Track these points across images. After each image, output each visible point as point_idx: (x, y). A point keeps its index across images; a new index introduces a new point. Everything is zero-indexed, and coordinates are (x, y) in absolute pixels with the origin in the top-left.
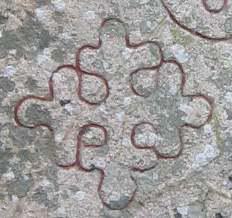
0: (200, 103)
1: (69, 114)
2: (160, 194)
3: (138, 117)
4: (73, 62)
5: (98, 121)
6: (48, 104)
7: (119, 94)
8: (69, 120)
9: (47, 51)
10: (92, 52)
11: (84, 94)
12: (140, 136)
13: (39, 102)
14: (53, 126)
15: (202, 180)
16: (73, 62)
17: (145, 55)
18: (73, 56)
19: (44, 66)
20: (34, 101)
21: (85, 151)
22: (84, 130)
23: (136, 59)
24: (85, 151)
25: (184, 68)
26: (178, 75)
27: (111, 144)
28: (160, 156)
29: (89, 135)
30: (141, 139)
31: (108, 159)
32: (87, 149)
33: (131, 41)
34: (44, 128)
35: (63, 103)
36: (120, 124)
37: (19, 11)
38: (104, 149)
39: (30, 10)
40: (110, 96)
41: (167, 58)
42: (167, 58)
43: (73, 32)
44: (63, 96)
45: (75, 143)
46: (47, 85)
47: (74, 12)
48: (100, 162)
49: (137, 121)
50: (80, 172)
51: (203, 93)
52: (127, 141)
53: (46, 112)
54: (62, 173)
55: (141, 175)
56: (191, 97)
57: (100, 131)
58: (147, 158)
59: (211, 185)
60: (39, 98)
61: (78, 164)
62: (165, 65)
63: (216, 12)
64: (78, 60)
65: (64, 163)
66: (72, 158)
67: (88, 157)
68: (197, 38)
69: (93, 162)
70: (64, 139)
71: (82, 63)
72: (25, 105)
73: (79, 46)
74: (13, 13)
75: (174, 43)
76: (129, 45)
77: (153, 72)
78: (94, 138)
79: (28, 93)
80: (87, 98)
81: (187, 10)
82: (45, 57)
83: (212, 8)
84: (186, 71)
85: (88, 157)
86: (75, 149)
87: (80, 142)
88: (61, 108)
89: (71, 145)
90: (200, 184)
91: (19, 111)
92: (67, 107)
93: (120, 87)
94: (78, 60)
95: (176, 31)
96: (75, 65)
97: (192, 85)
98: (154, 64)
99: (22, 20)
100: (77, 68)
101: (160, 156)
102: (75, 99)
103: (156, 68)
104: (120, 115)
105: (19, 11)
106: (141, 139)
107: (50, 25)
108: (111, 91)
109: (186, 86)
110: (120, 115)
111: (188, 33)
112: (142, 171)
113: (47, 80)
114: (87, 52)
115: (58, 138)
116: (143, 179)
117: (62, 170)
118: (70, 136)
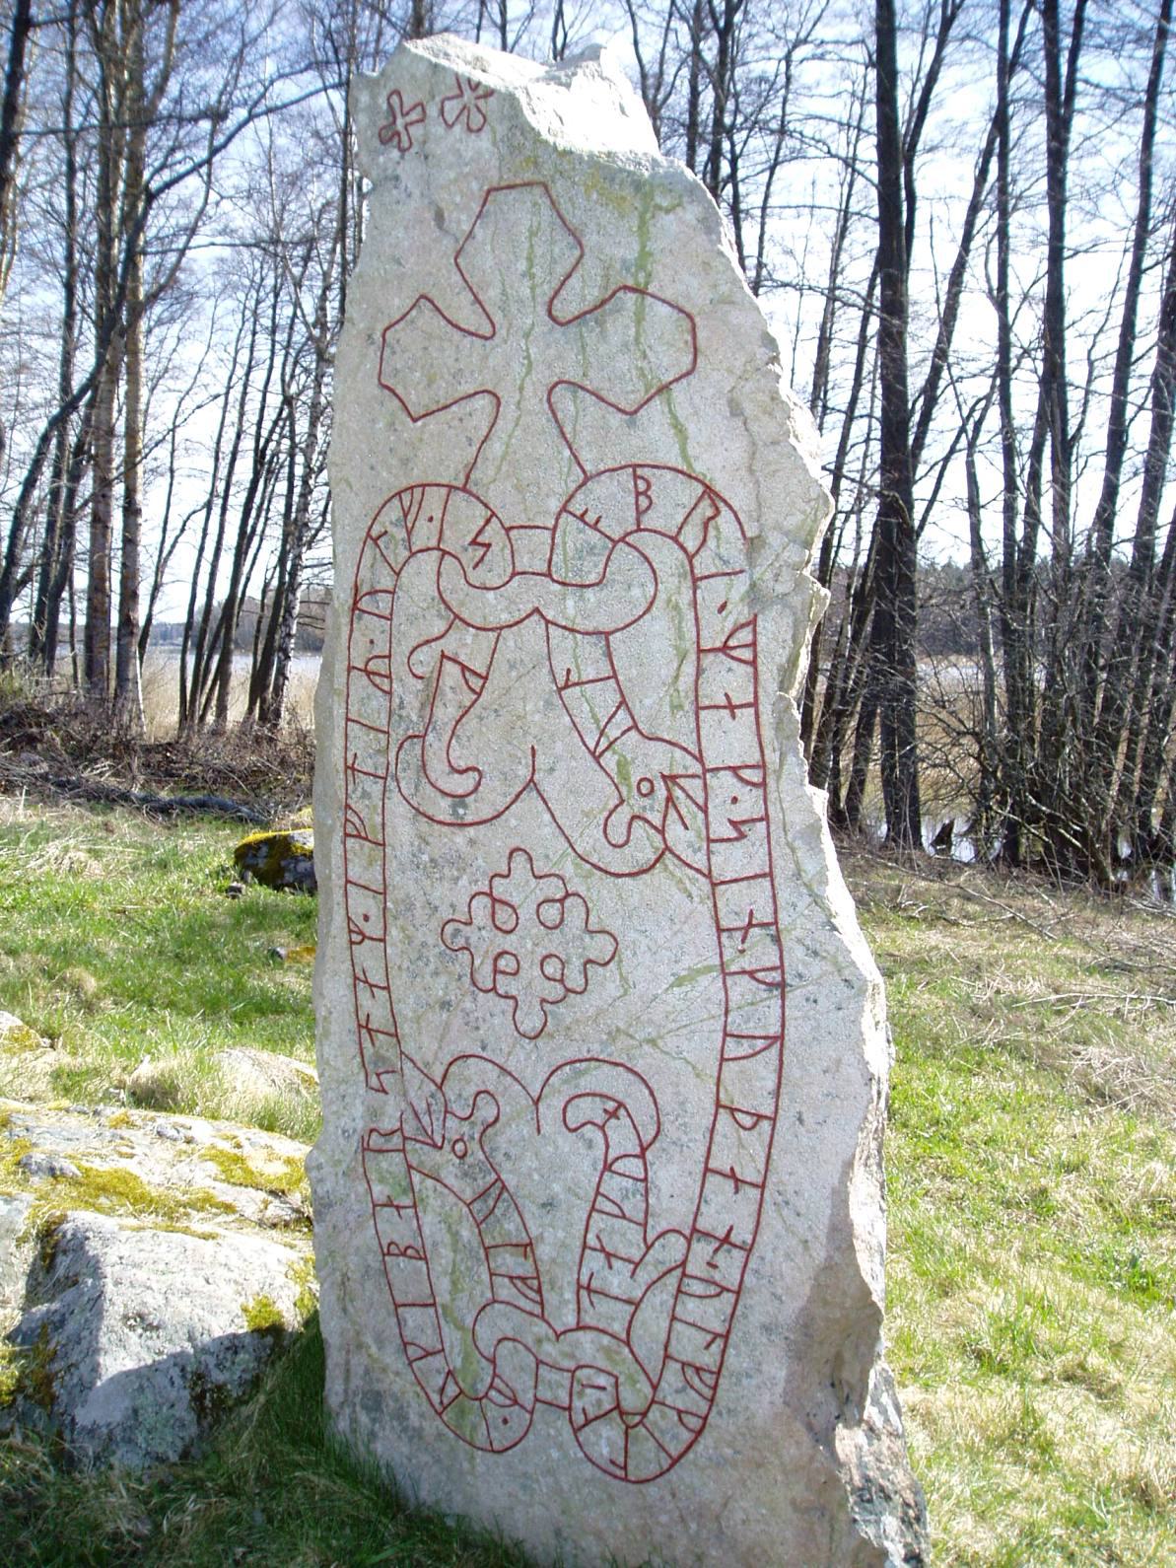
22: (500, 955)
27: (522, 973)
30: (549, 970)
52: (537, 972)
61: (494, 989)
72: (449, 928)
87: (496, 971)
106: (549, 970)
114: (497, 880)
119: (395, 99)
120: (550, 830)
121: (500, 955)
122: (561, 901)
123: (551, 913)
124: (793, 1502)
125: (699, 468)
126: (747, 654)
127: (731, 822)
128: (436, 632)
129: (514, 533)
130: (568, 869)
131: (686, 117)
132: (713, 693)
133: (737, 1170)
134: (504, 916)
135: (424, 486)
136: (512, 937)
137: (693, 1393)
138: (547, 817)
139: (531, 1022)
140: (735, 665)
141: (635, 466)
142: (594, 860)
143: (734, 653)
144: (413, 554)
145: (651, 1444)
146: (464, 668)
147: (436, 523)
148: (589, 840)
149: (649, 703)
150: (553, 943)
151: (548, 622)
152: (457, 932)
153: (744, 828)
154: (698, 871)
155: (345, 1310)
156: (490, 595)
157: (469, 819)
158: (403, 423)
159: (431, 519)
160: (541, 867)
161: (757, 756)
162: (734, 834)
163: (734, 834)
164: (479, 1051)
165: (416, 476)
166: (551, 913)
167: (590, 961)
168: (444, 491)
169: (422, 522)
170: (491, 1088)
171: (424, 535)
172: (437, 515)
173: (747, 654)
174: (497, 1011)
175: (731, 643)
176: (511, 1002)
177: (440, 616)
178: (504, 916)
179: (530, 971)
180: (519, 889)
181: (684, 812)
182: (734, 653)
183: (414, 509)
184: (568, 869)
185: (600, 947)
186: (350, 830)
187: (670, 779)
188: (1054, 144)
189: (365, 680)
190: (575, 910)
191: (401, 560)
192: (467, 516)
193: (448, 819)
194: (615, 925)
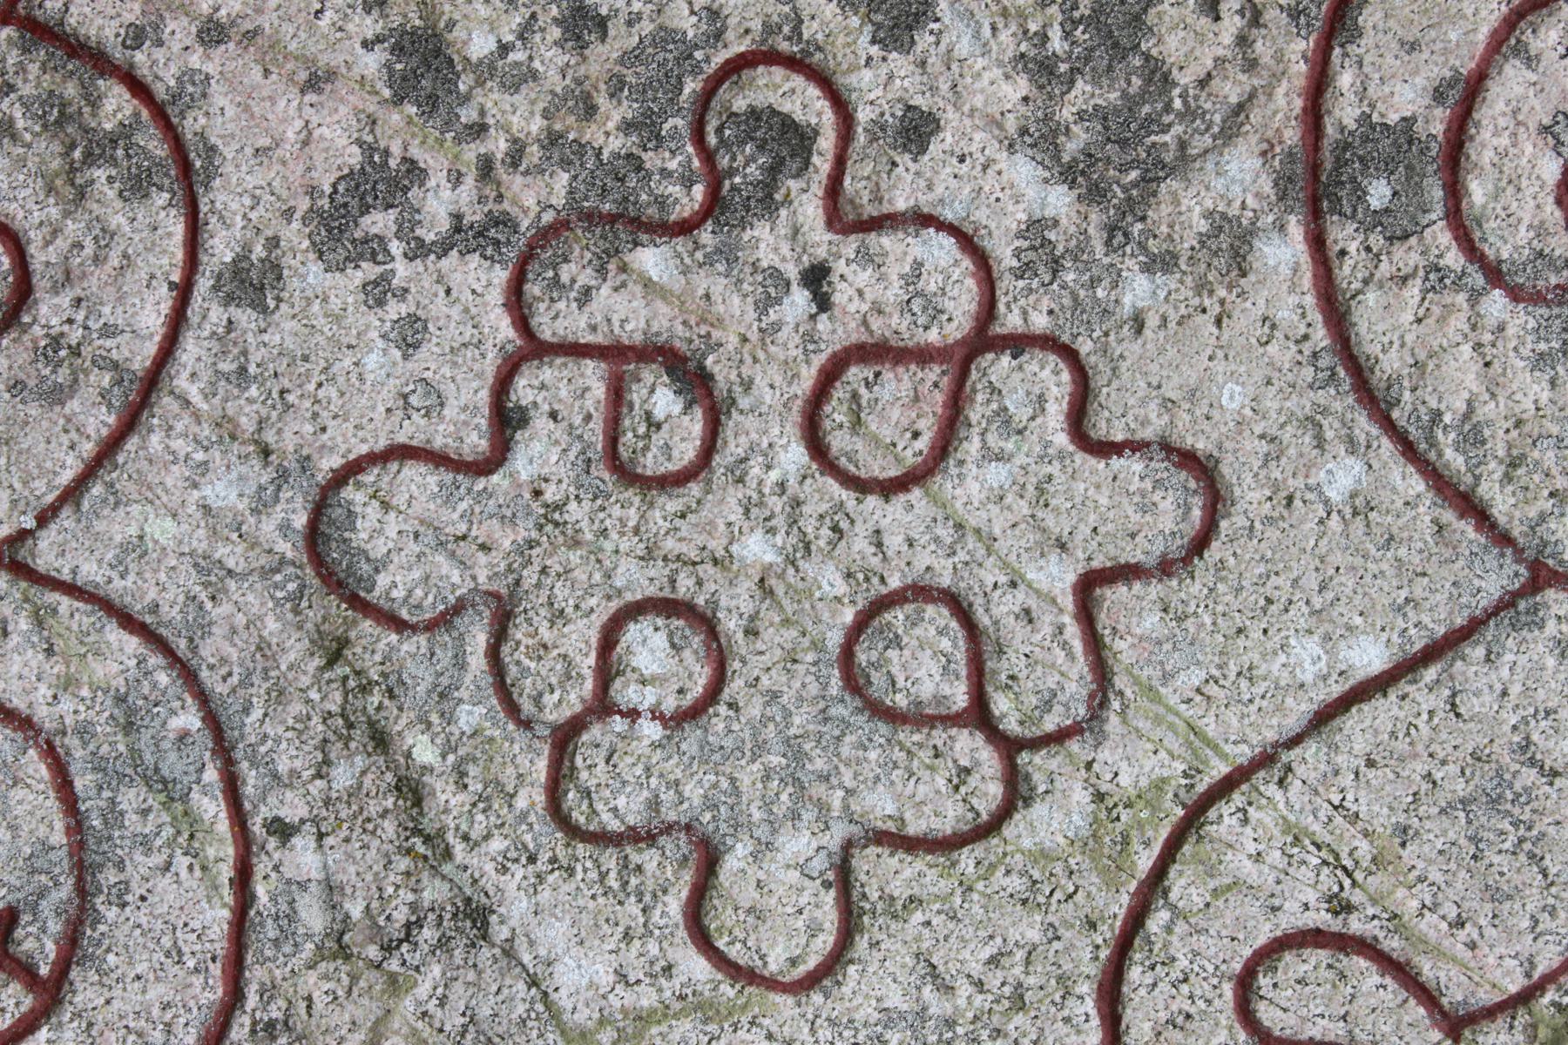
0: (814, 930)
1: (765, 304)
2: (380, 740)
3: (751, 632)
4: (1010, 321)
5: (733, 447)
6: (810, 208)
7: (860, 544)
8: (736, 308)
9: (1060, 201)
10: (1056, 413)
11: (855, 374)
12: (660, 640)
13: (822, 165)
14: (706, 236)
15: (443, 943)
16: (1010, 321)
17: (1042, 671)
18: (1040, 322)
19: (989, 182)
20: (827, 142)
21: (593, 375)
22: (692, 378)
23: (1027, 615)
24: (593, 375)
25: (979, 850)
26: (948, 817)
27: (626, 507)
28: (565, 738)
29: (665, 401)
30: (647, 646)
31: (551, 494)
32: (599, 391)
33: (1115, 596)
34: (699, 191)
35: (816, 277)
36: (717, 545)
37: (1251, 65)
38: (601, 472)
39: (1255, 117)
40: (847, 496)
41: (1036, 763)
42: (1036, 763)
43: (1152, 321)
44: (853, 285)
45: (633, 331)
46: (901, 204)
47: (1245, 319)
48: (537, 455)
49: (731, 625)
50: (490, 364)
51: (861, 944)
52: (638, 580)
53: (767, 201)
54: (482, 280)
55: (477, 661)
56: (843, 878)
57: (686, 452)
58: (557, 676)
59: (423, 990)
60: (840, 163)
61: (534, 347)
62: (989, 759)
63: (668, 607)
64: (1018, 344)
65: (533, 289)
66: (558, 320)
67: (565, 393)
68: (1119, 906)
69: (541, 423)
70: (647, 284)
71: (1006, 360)
72: (805, 103)
73: (1085, 347)
74: (1242, 41)
75: (1099, 797)
76: (1089, 586)
77: (959, 696)
78: (654, 425)
79: (864, 115)
80: (839, 393)
81: (1258, 857)
82: (1019, 194)
83: (1264, 981)
84: (967, 859)
85: (565, 393)
86: (598, 339)
87: (619, 357)
88: (792, 272)
89: (623, 313)
90: (428, 934)
91: (778, 72)
92: (799, 300)
93: (894, 542)
94: (1018, 344)
95: (1154, 807)
96: (997, 329)
97: (898, 889)
98: (1001, 704)
99: (1203, 83)
100: (985, 338)
101: (565, 738)
102: (835, 333)
103: (979, 715)
104: (757, 549)
105: (1251, 65)
106: (647, 646)
107: (1186, 209)
108: (872, 501)
109: (892, 861)
110: (757, 549)
111: (1145, 861)
112: (494, 654)
113: (925, 201)
114: (1054, 380)
115: (651, 259)
116: (460, 664)
117: (501, 275)
118: (662, 308)
120: (1308, 665)
122: (979, 715)
123: (923, 663)
130: (1138, 759)
131: (66, 512)
134: (896, 411)
136: (794, 456)
138: (1370, 657)
139: (396, 533)
142: (1183, 885)
148: (1256, 871)
150: (782, 677)
152: (792, 140)
160: (1133, 614)
164: (221, 248)
166: (923, 663)
167: (709, 859)
170: (49, 310)
176: (476, 442)
179: (625, 549)
180: (1018, 508)
184: (1138, 759)
185: (778, 897)
188: (1276, 945)
190: (933, 786)
193: (1344, 113)
194: (878, 983)
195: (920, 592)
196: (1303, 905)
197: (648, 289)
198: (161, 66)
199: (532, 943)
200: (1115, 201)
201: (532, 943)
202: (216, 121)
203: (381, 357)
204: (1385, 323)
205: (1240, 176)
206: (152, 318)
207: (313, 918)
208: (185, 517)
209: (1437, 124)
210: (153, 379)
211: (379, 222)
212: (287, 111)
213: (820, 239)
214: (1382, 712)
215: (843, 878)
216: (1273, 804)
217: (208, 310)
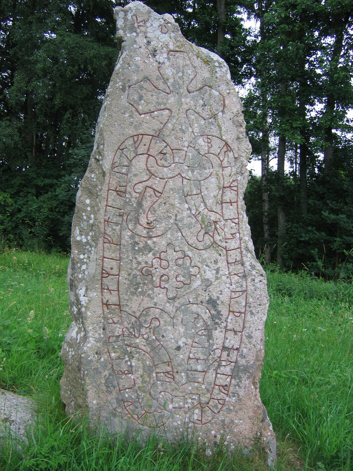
5: (166, 274)
8: (157, 274)
9: (151, 253)
17: (180, 254)
21: (162, 282)
22: (162, 276)
26: (189, 260)
27: (170, 281)
28: (184, 284)
29: (163, 278)
30: (178, 279)
35: (156, 269)
44: (156, 266)
48: (166, 286)
52: (174, 280)
54: (155, 289)
61: (160, 286)
64: (160, 256)
82: (150, 255)
87: (161, 280)
89: (158, 280)
94: (160, 256)
100: (160, 258)
101: (184, 284)
102: (159, 267)
103: (183, 258)
104: (172, 272)
106: (178, 279)
114: (163, 253)
115: (154, 279)
119: (134, 18)
121: (162, 276)
124: (249, 417)
125: (224, 138)
126: (235, 189)
127: (231, 234)
128: (145, 179)
129: (174, 151)
132: (227, 198)
133: (235, 329)
135: (143, 135)
137: (222, 393)
140: (232, 191)
141: (207, 135)
142: (194, 245)
143: (233, 188)
144: (137, 155)
145: (210, 411)
146: (154, 190)
147: (147, 147)
148: (192, 240)
149: (210, 202)
151: (183, 177)
153: (234, 235)
154: (223, 247)
155: (99, 397)
156: (165, 169)
157: (153, 236)
158: (136, 115)
159: (145, 145)
161: (116, 286)
162: (232, 237)
163: (232, 237)
164: (153, 306)
165: (141, 131)
166: (180, 262)
168: (151, 137)
169: (142, 145)
170: (157, 316)
171: (142, 149)
172: (148, 144)
173: (235, 189)
174: (161, 293)
175: (232, 185)
177: (147, 175)
178: (164, 263)
180: (172, 255)
181: (219, 231)
182: (233, 188)
183: (138, 142)
186: (106, 241)
187: (216, 222)
189: (115, 193)
191: (132, 157)
192: (157, 147)
193: (146, 236)
195: (175, 262)
196: (195, 238)
197: (156, 279)
198: (142, 309)
199: (169, 460)
200: (321, 205)
201: (169, 460)
202: (146, 306)
203: (160, 296)
204: (160, 233)
205: (149, 242)
206: (158, 310)
207: (195, 299)
208: (169, 308)
209: (147, 230)
210: (162, 310)
211: (152, 296)
212: (145, 302)
213: (153, 268)
214: (183, 233)
215: (193, 267)
216: (188, 240)
217: (157, 306)
